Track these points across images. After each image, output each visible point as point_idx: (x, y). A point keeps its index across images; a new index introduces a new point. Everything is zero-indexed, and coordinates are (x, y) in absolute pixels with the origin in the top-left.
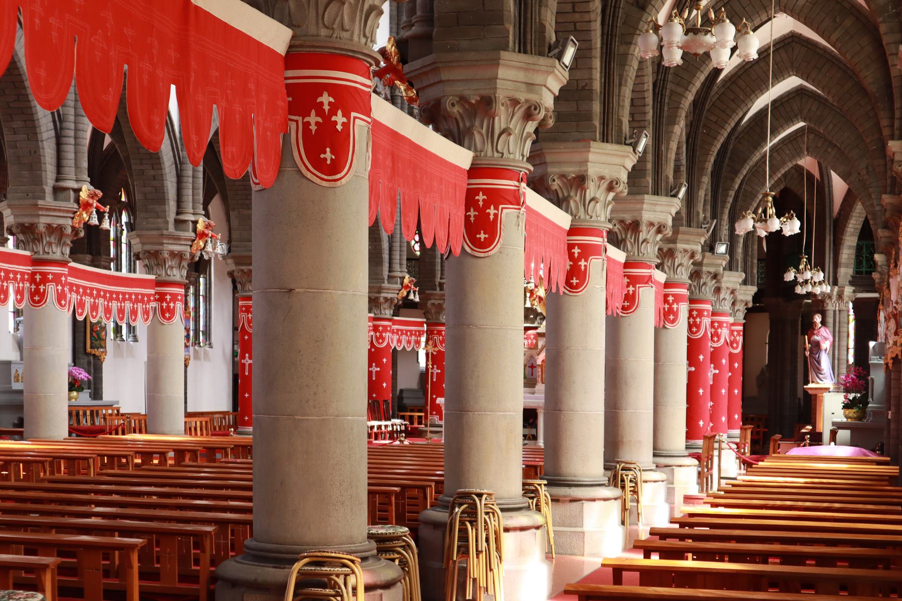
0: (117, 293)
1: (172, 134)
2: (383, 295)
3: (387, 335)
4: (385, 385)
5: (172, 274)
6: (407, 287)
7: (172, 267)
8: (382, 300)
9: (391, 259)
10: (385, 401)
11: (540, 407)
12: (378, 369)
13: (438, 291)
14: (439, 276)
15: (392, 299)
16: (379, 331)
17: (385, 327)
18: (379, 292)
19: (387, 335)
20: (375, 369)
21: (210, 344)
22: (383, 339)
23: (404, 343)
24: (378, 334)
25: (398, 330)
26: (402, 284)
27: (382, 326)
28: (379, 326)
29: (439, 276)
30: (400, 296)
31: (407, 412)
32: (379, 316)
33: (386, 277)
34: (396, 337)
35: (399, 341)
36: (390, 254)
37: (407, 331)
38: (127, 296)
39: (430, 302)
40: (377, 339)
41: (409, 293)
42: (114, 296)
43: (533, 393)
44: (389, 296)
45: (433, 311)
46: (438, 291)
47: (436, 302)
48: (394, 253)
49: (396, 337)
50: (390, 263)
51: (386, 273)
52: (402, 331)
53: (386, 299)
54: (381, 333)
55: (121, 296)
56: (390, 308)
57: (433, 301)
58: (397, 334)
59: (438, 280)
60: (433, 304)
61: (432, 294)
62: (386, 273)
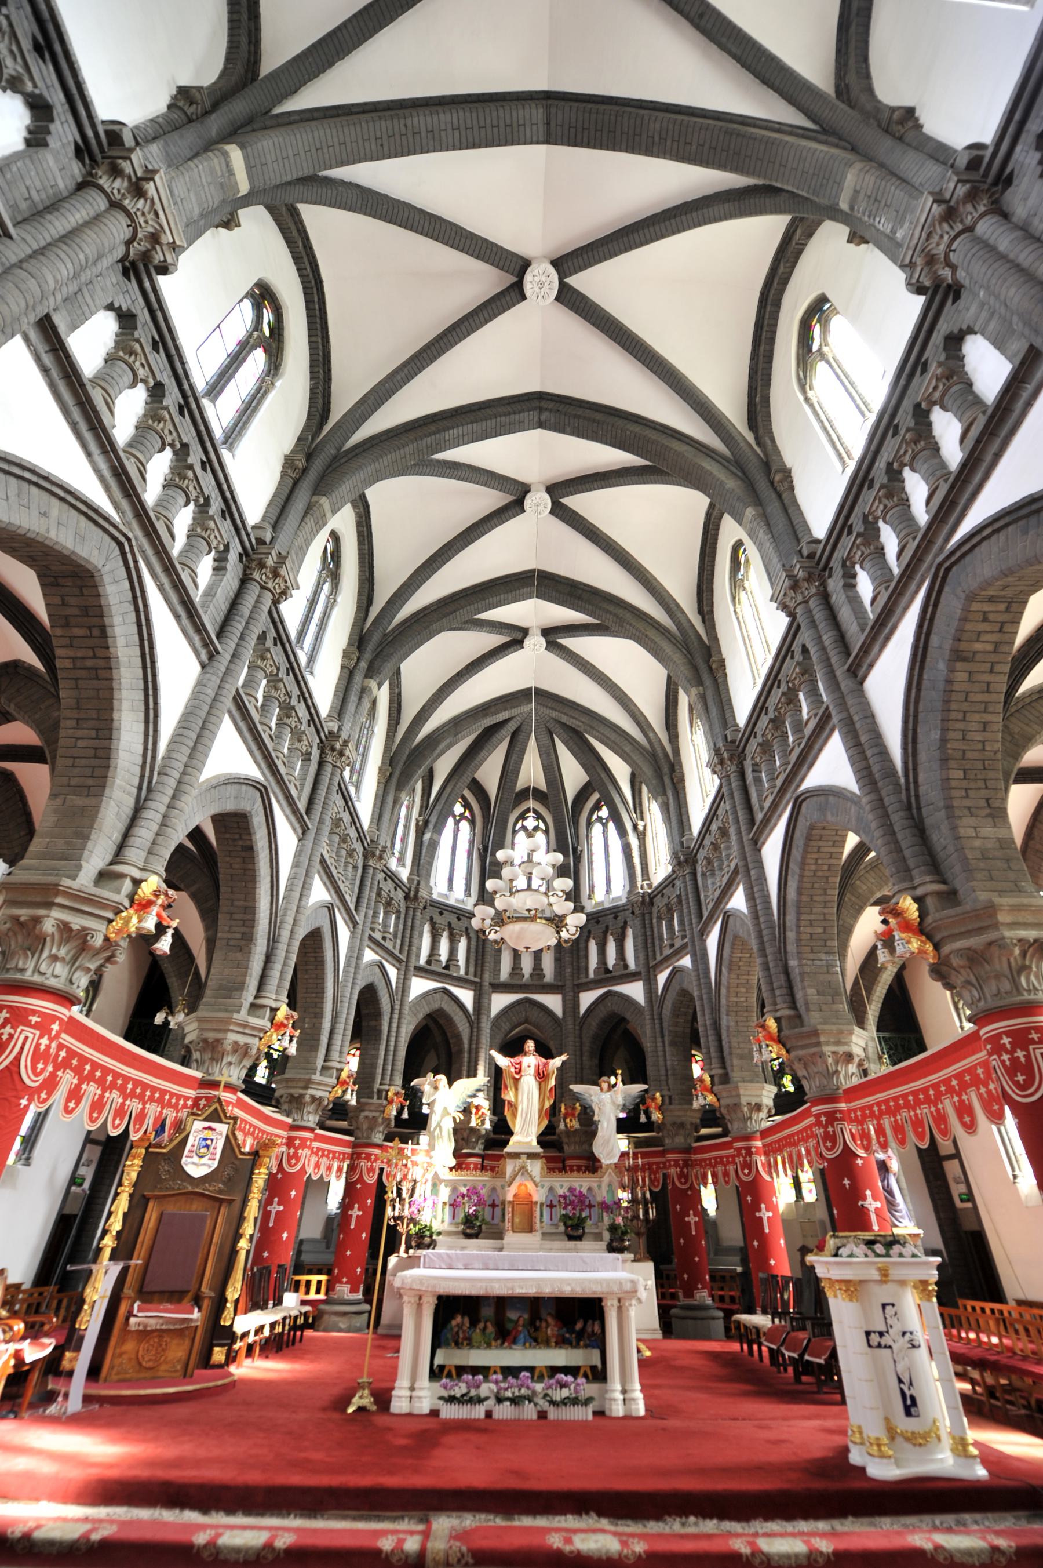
0: (106, 1071)
1: (146, 643)
2: (311, 1092)
3: (304, 1153)
4: (285, 1235)
5: (49, 972)
6: (345, 1083)
7: (54, 958)
8: (307, 1098)
9: (329, 1045)
10: (280, 1266)
11: (612, 1293)
12: (281, 1208)
13: (375, 1100)
14: (378, 1080)
15: (321, 1099)
16: (293, 1146)
17: (304, 1140)
18: (306, 1088)
19: (304, 1153)
20: (276, 1208)
21: (28, 1159)
22: (298, 1159)
23: (323, 1170)
24: (292, 1151)
25: (319, 1149)
26: (338, 1078)
27: (301, 1138)
28: (295, 1138)
29: (378, 1080)
30: (332, 1097)
31: (303, 1274)
32: (299, 1123)
33: (319, 1068)
34: (314, 1159)
35: (317, 1166)
36: (330, 1038)
37: (329, 1152)
38: (75, 1062)
39: (363, 1114)
40: (289, 1158)
41: (344, 1092)
42: (120, 1082)
43: (501, 1249)
44: (318, 1094)
45: (365, 1126)
46: (375, 1100)
47: (371, 1115)
48: (335, 1036)
49: (314, 1159)
50: (328, 1050)
51: (320, 1062)
52: (323, 1150)
53: (313, 1098)
54: (296, 1149)
55: (110, 1078)
56: (316, 1112)
57: (366, 1113)
58: (317, 1154)
59: (377, 1086)
60: (367, 1117)
61: (367, 1104)
62: (320, 1062)
